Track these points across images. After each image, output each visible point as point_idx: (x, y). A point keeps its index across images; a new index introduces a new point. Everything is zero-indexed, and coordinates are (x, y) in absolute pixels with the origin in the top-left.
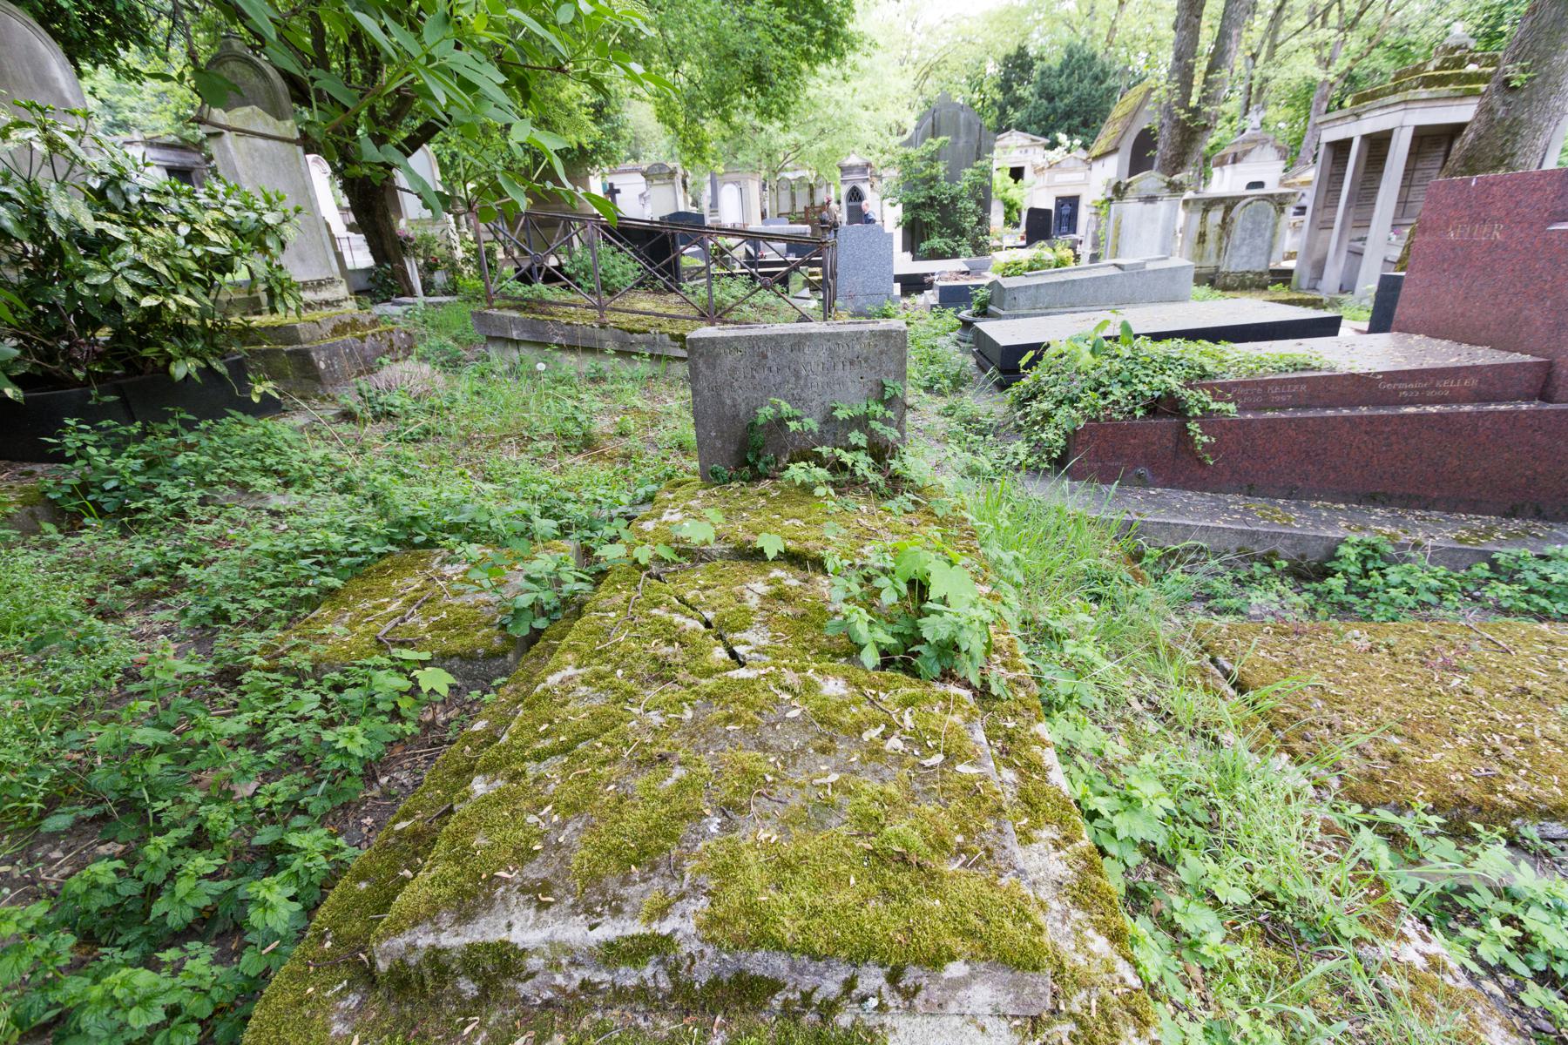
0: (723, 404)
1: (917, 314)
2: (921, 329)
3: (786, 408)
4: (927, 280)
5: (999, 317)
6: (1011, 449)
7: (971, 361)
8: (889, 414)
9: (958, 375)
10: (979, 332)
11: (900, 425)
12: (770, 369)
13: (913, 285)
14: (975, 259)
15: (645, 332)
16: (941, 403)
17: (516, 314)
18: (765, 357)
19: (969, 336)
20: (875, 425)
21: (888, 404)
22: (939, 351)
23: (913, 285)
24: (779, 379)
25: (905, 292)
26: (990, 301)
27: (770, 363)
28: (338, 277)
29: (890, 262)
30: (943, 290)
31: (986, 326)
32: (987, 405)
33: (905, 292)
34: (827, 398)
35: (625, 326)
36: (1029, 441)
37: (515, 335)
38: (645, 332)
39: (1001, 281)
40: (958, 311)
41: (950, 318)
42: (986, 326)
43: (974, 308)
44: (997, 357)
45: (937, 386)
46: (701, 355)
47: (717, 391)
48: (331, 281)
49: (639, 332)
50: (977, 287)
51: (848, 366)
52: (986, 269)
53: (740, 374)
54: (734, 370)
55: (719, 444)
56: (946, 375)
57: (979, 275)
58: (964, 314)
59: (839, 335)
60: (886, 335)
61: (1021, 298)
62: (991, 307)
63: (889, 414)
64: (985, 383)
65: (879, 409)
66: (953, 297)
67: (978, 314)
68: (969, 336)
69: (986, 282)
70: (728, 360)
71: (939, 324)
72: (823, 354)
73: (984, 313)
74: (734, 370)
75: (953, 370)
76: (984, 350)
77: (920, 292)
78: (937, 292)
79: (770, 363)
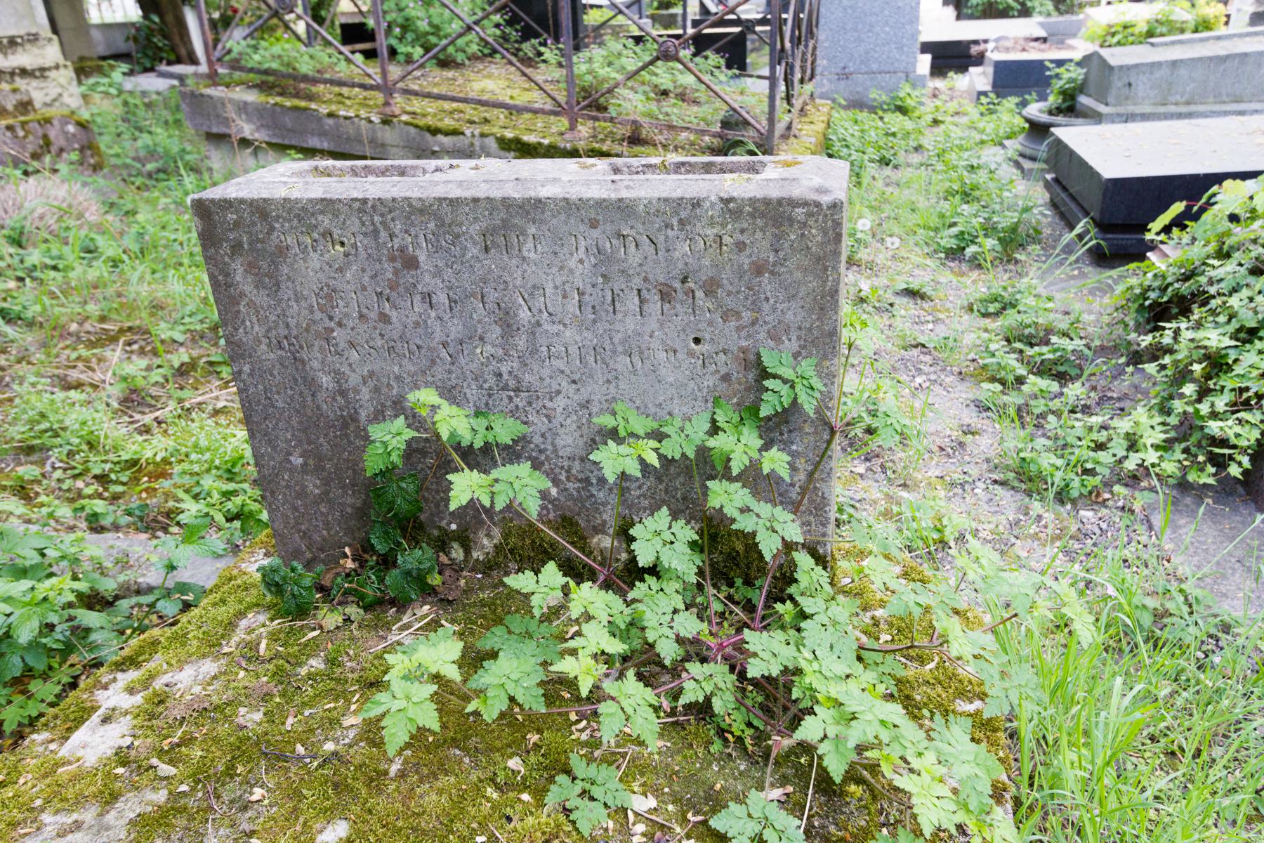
0: (312, 385)
1: (952, 107)
2: (956, 133)
3: (453, 423)
4: (974, 50)
5: (1096, 118)
6: (1124, 425)
7: (1040, 195)
8: (776, 461)
9: (1014, 229)
10: (1060, 147)
11: (806, 498)
12: (428, 297)
13: (951, 58)
14: (1056, 19)
15: (455, 132)
16: (976, 285)
17: (252, 97)
18: (412, 264)
19: (1043, 149)
20: (725, 497)
21: (777, 428)
22: (981, 177)
23: (951, 58)
24: (456, 329)
25: (938, 69)
26: (1082, 88)
27: (427, 281)
28: (46, 31)
29: (914, 19)
30: (1000, 67)
31: (1073, 135)
32: (1078, 299)
33: (938, 69)
34: (595, 390)
35: (429, 121)
36: (1165, 410)
37: (247, 129)
38: (455, 132)
39: (1105, 53)
40: (1024, 104)
41: (1010, 115)
42: (1073, 135)
43: (1053, 100)
44: (1094, 200)
45: (970, 250)
46: (237, 247)
47: (292, 350)
48: (34, 38)
49: (447, 134)
50: (1060, 63)
51: (654, 306)
52: (1074, 35)
53: (348, 306)
54: (330, 294)
55: (313, 486)
56: (989, 229)
57: (1061, 44)
58: (1036, 110)
59: (623, 208)
60: (775, 214)
61: (1142, 86)
62: (1083, 100)
63: (776, 461)
64: (1068, 250)
65: (740, 446)
66: (1017, 78)
67: (1059, 111)
68: (1043, 149)
69: (1077, 56)
70: (311, 267)
71: (989, 126)
72: (579, 266)
73: (1070, 108)
74: (330, 294)
75: (1006, 220)
76: (1069, 182)
77: (963, 69)
78: (990, 70)
79: (427, 281)
